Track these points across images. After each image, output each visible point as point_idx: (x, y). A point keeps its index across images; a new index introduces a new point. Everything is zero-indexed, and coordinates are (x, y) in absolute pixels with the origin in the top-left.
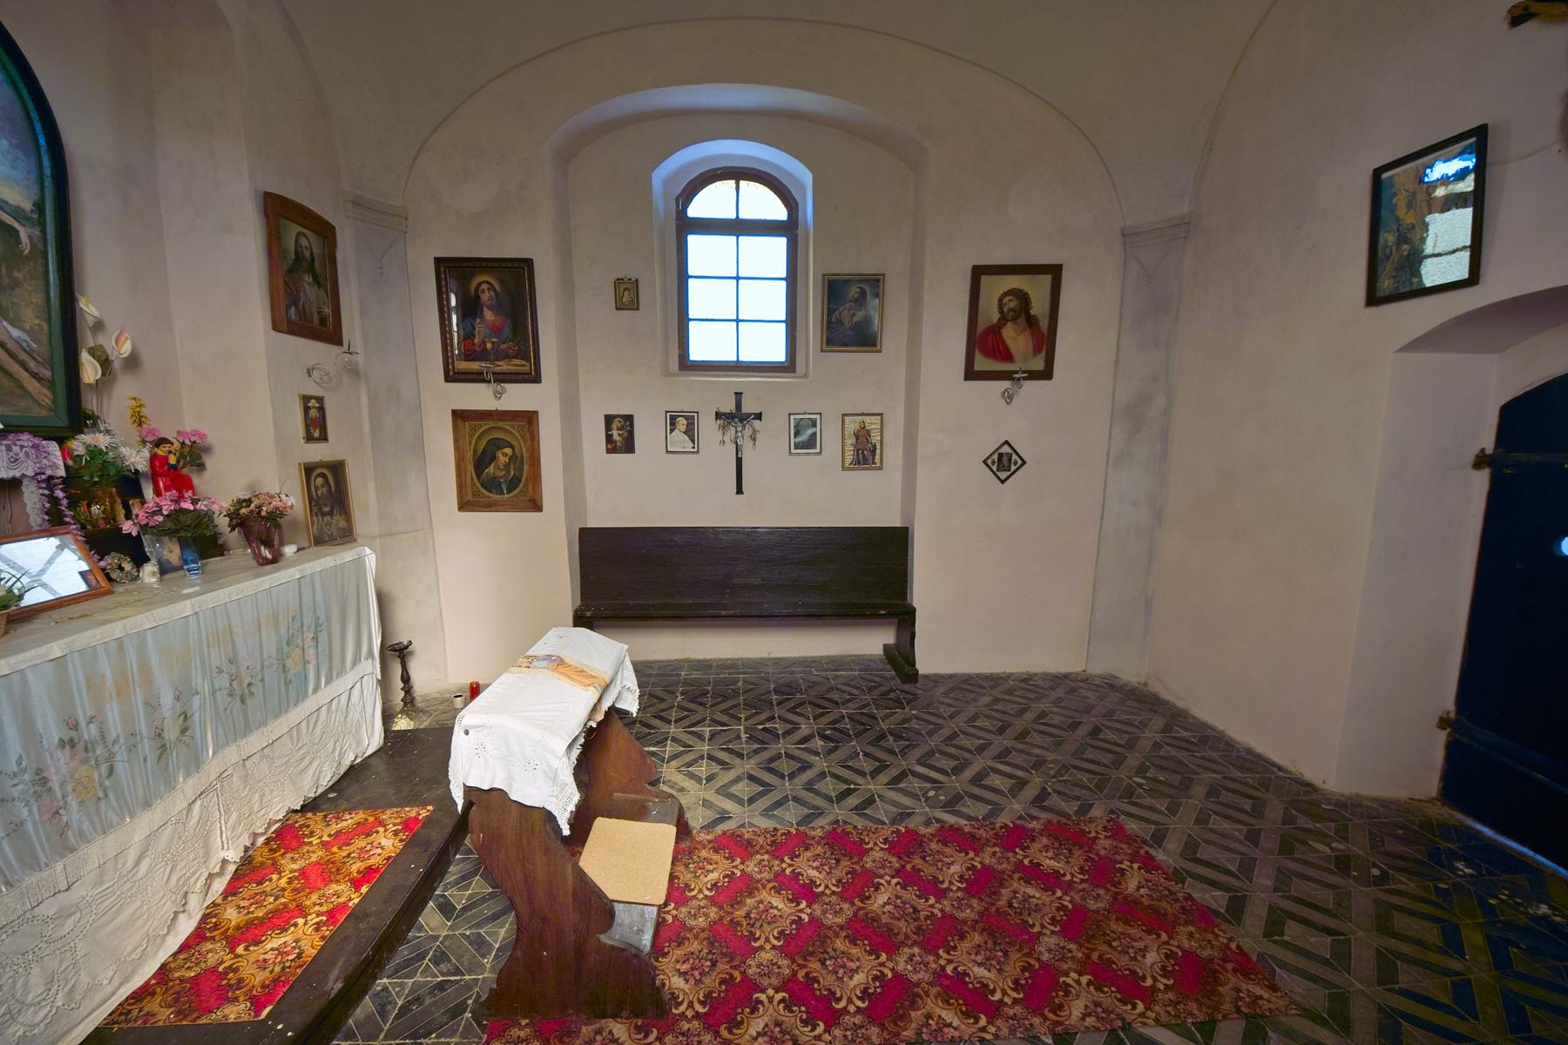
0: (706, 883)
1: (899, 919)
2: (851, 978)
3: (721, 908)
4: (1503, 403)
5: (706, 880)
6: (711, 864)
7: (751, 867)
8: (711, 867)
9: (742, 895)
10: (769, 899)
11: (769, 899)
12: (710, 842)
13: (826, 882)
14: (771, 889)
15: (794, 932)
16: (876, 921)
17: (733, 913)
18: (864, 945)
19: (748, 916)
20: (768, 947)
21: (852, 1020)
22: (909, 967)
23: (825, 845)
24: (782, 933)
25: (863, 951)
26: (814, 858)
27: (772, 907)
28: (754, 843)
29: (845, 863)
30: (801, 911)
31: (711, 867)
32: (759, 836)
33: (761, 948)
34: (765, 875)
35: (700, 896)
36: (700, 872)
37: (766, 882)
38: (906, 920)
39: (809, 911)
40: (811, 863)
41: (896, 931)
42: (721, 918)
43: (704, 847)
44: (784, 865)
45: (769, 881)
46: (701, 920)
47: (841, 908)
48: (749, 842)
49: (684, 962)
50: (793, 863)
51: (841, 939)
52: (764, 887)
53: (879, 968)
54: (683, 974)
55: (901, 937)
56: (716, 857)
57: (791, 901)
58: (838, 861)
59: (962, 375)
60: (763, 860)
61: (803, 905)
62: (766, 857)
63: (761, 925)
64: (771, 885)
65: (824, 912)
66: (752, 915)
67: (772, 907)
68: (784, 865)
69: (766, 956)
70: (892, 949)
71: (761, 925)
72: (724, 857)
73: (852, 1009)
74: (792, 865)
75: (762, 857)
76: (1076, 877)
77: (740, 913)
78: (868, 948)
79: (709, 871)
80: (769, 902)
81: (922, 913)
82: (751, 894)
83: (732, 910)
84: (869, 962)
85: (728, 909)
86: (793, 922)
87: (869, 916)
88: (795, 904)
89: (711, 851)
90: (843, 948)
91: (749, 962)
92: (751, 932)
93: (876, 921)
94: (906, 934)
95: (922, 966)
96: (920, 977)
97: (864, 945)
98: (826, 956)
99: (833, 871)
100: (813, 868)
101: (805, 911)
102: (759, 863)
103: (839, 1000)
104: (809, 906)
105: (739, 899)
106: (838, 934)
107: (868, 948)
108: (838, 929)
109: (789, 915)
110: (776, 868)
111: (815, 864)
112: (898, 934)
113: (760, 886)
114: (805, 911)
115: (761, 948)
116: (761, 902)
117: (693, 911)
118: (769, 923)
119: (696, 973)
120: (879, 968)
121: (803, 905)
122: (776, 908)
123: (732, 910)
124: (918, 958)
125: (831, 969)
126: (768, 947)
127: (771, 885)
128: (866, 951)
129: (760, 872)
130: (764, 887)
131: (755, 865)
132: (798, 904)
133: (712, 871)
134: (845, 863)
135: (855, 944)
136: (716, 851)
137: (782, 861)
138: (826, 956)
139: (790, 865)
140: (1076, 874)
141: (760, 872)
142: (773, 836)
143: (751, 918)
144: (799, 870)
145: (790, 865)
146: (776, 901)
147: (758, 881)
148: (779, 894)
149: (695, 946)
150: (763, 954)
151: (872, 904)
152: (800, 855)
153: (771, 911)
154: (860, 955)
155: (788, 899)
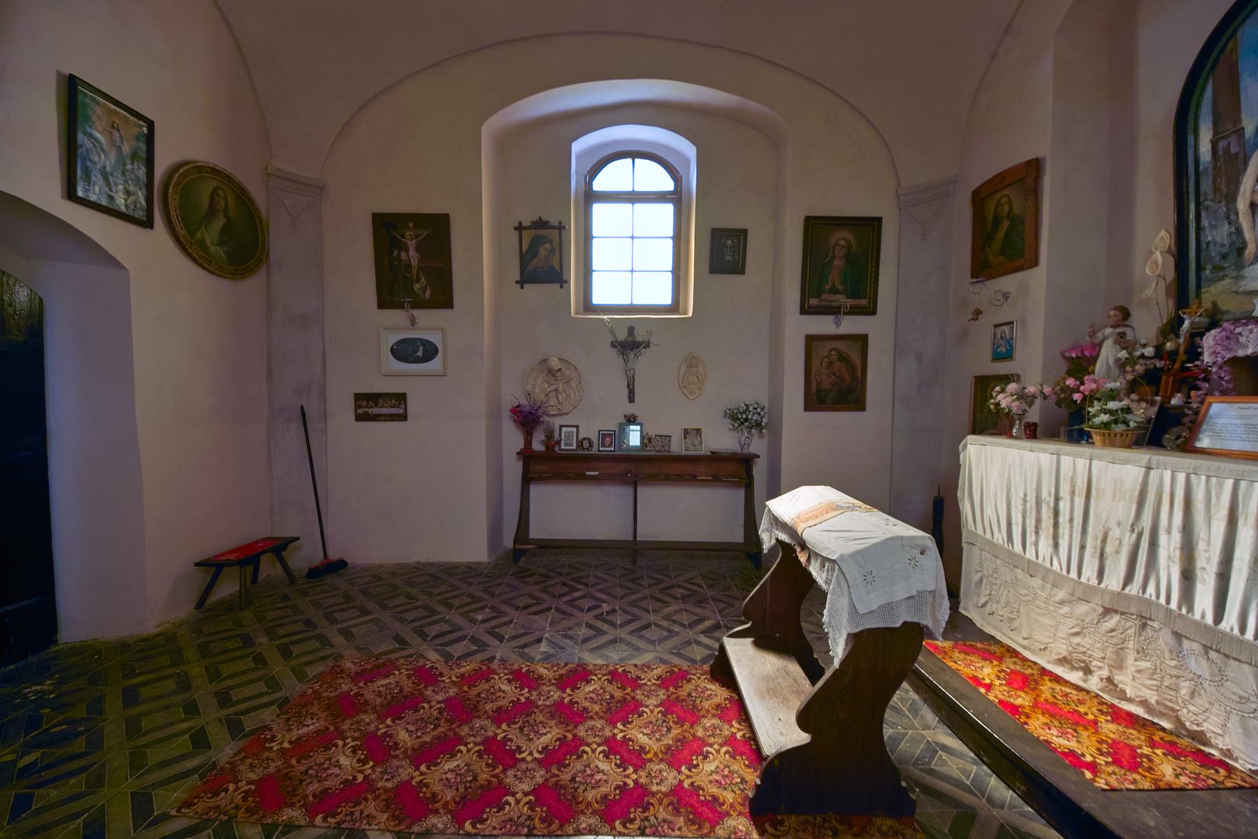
0: (714, 760)
1: (664, 821)
2: (717, 767)
3: (694, 736)
4: (973, 189)
5: (596, 686)
6: (591, 698)
7: (671, 777)
8: (591, 695)
9: (677, 747)
10: (651, 742)
11: (651, 742)
12: (592, 718)
13: (593, 756)
14: (649, 752)
15: (694, 758)
16: (689, 820)
17: (683, 731)
18: (705, 796)
19: (669, 729)
20: (651, 707)
21: (716, 740)
22: (665, 774)
23: (581, 802)
24: (640, 715)
25: (706, 790)
26: (599, 784)
27: (648, 735)
28: (670, 808)
29: (566, 777)
30: (622, 731)
31: (591, 695)
32: (541, 722)
33: (657, 706)
34: (655, 767)
35: (600, 676)
36: (600, 692)
37: (654, 759)
38: (657, 819)
39: (616, 731)
40: (605, 777)
41: (670, 808)
42: (692, 726)
43: (597, 713)
44: (634, 776)
45: (650, 760)
46: (709, 725)
47: (587, 731)
48: (552, 717)
49: (600, 780)
50: (624, 779)
51: (727, 803)
52: (656, 754)
53: (692, 774)
54: (340, 767)
55: (666, 801)
56: (586, 704)
57: (630, 740)
58: (573, 780)
59: (883, 220)
60: (657, 784)
61: (619, 737)
62: (654, 788)
63: (657, 721)
64: (649, 756)
65: (602, 729)
66: (665, 729)
67: (648, 735)
68: (634, 776)
69: (653, 701)
70: (677, 791)
71: (657, 721)
72: (578, 704)
73: (716, 746)
74: (625, 776)
75: (659, 788)
76: (365, 770)
77: (676, 731)
78: (701, 792)
79: (593, 692)
80: (651, 739)
81: (636, 827)
82: (669, 748)
83: (684, 734)
84: (701, 780)
85: (687, 735)
86: (630, 723)
87: (697, 826)
88: (696, 784)
89: (647, 749)
90: (725, 793)
91: (665, 697)
92: (665, 716)
93: (689, 820)
94: (660, 804)
95: (653, 775)
96: (657, 767)
97: (705, 796)
98: (741, 786)
99: (582, 768)
100: (603, 772)
101: (619, 732)
102: (548, 698)
103: (727, 752)
104: (615, 735)
105: (679, 744)
106: (731, 807)
107: (701, 792)
108: (732, 812)
109: (633, 728)
110: (643, 774)
111: (598, 777)
112: (669, 804)
113: (660, 756)
114: (619, 732)
115: (657, 706)
116: (658, 740)
117: (718, 732)
118: (651, 722)
119: (589, 772)
120: (692, 774)
121: (619, 737)
122: (644, 734)
123: (684, 734)
124: (654, 781)
125: (735, 775)
126: (651, 707)
127: (649, 756)
128: (703, 789)
129: (660, 771)
130: (656, 754)
131: (666, 779)
132: (624, 737)
133: (590, 692)
134: (566, 777)
135: (713, 796)
136: (585, 709)
137: (636, 782)
138: (741, 786)
139: (628, 776)
140: (363, 768)
141: (660, 771)
142: (528, 722)
143: (667, 727)
144: (618, 770)
145: (628, 776)
146: (643, 739)
147: (662, 760)
148: (641, 747)
149: (706, 705)
150: (655, 703)
151: (558, 734)
152: (615, 789)
153: (649, 732)
154: (709, 786)
155: (633, 741)
